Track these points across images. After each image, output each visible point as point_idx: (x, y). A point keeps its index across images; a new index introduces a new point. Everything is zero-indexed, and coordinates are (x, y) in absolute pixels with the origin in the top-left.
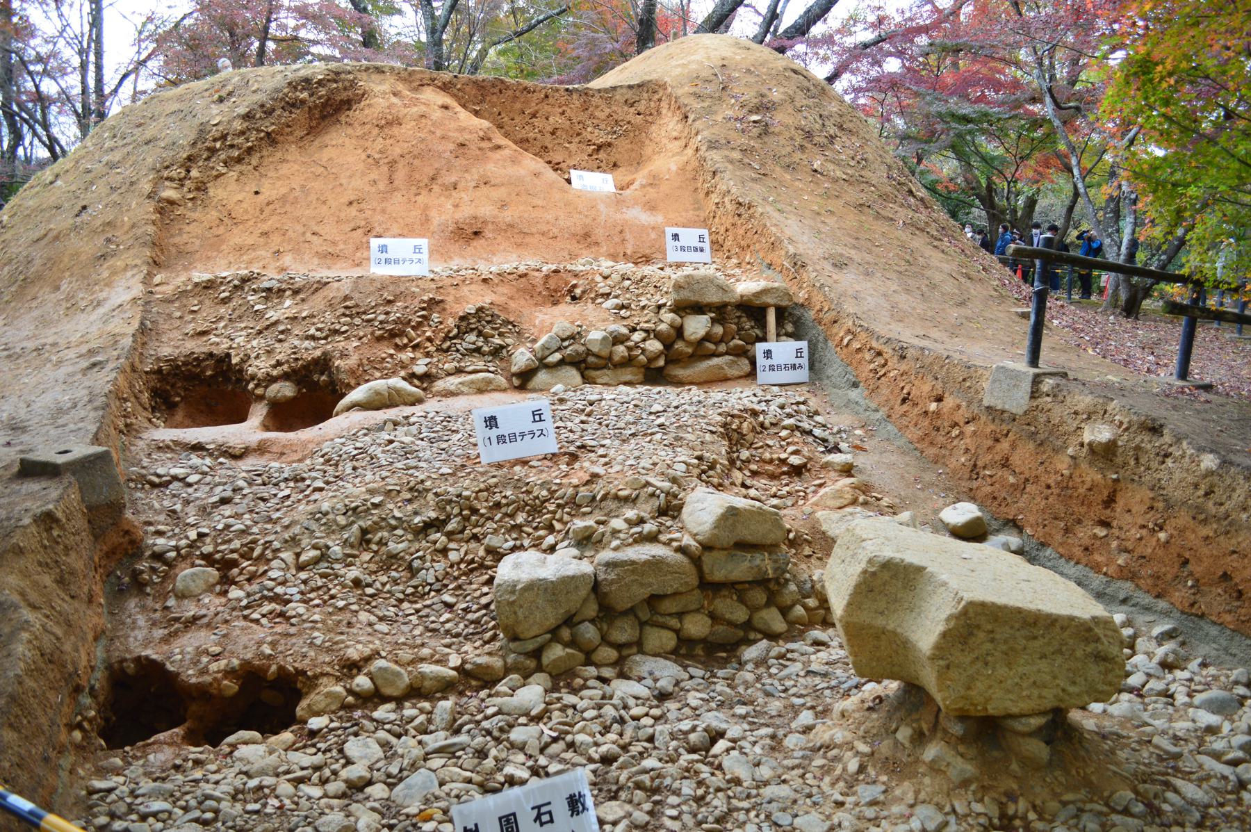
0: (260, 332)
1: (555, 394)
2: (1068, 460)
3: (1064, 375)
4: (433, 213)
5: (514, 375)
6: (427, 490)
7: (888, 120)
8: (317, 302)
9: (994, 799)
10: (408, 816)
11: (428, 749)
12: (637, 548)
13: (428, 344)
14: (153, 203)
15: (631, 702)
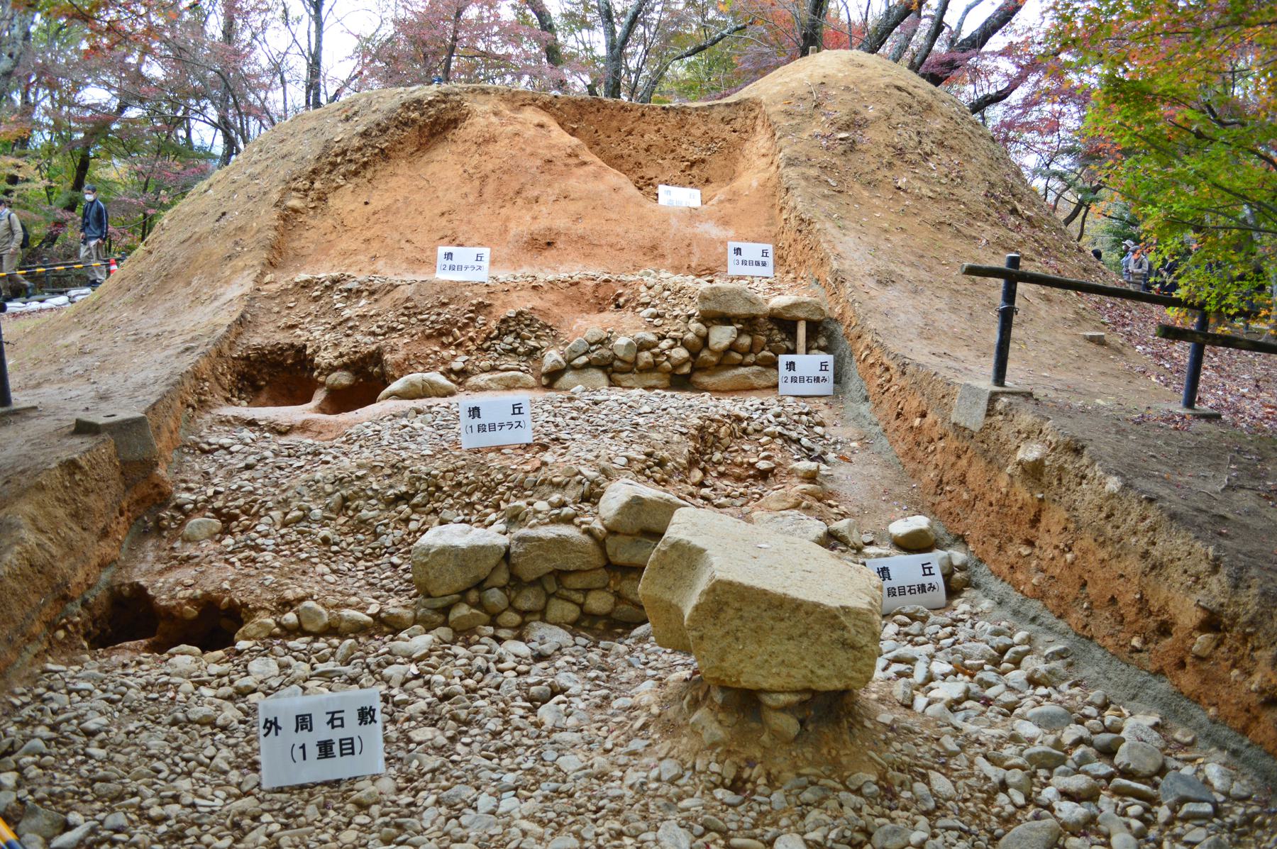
0: (334, 327)
2: (1007, 478)
5: (543, 374)
6: (405, 468)
8: (386, 302)
9: (734, 763)
13: (470, 343)
14: (278, 211)
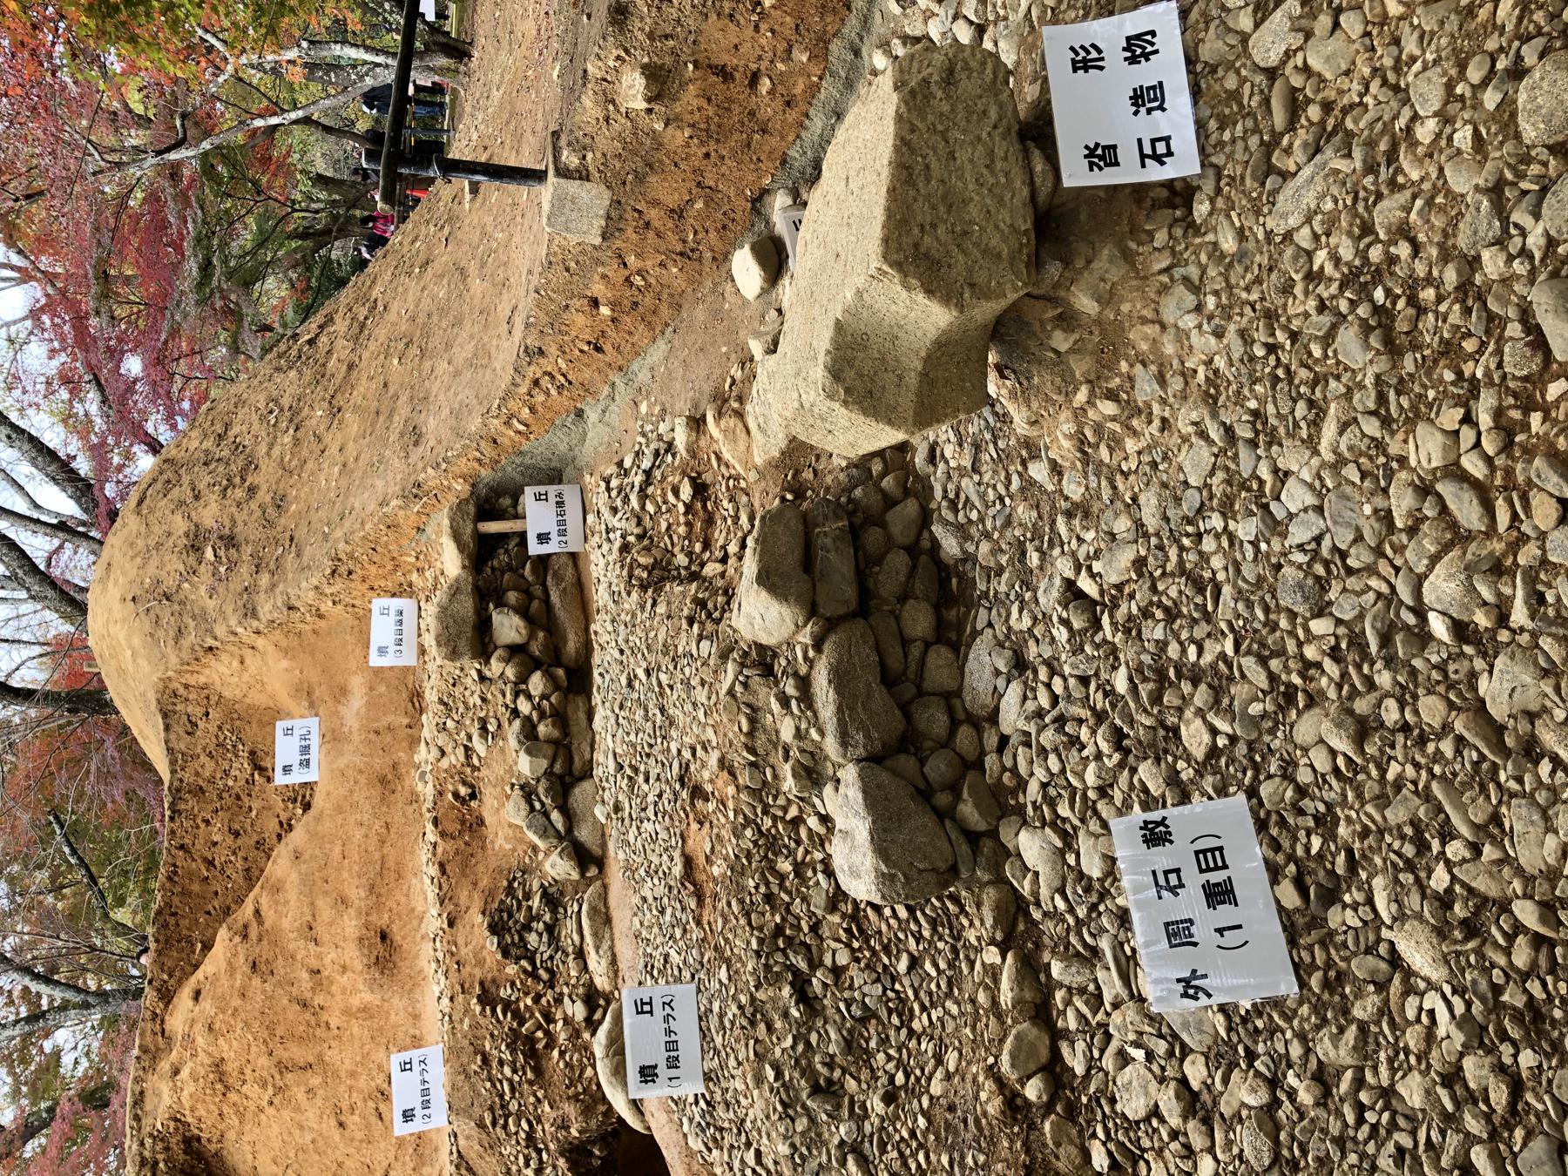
1: (608, 816)
2: (670, 130)
3: (556, 135)
4: (355, 1002)
5: (582, 874)
6: (753, 999)
7: (210, 370)
9: (1148, 217)
10: (1229, 1029)
11: (1125, 994)
12: (819, 705)
13: (544, 1001)
15: (1031, 706)
